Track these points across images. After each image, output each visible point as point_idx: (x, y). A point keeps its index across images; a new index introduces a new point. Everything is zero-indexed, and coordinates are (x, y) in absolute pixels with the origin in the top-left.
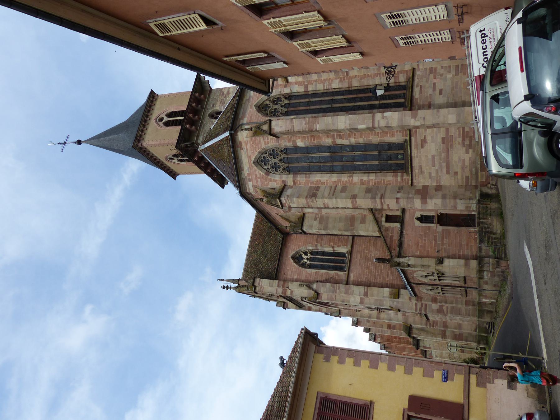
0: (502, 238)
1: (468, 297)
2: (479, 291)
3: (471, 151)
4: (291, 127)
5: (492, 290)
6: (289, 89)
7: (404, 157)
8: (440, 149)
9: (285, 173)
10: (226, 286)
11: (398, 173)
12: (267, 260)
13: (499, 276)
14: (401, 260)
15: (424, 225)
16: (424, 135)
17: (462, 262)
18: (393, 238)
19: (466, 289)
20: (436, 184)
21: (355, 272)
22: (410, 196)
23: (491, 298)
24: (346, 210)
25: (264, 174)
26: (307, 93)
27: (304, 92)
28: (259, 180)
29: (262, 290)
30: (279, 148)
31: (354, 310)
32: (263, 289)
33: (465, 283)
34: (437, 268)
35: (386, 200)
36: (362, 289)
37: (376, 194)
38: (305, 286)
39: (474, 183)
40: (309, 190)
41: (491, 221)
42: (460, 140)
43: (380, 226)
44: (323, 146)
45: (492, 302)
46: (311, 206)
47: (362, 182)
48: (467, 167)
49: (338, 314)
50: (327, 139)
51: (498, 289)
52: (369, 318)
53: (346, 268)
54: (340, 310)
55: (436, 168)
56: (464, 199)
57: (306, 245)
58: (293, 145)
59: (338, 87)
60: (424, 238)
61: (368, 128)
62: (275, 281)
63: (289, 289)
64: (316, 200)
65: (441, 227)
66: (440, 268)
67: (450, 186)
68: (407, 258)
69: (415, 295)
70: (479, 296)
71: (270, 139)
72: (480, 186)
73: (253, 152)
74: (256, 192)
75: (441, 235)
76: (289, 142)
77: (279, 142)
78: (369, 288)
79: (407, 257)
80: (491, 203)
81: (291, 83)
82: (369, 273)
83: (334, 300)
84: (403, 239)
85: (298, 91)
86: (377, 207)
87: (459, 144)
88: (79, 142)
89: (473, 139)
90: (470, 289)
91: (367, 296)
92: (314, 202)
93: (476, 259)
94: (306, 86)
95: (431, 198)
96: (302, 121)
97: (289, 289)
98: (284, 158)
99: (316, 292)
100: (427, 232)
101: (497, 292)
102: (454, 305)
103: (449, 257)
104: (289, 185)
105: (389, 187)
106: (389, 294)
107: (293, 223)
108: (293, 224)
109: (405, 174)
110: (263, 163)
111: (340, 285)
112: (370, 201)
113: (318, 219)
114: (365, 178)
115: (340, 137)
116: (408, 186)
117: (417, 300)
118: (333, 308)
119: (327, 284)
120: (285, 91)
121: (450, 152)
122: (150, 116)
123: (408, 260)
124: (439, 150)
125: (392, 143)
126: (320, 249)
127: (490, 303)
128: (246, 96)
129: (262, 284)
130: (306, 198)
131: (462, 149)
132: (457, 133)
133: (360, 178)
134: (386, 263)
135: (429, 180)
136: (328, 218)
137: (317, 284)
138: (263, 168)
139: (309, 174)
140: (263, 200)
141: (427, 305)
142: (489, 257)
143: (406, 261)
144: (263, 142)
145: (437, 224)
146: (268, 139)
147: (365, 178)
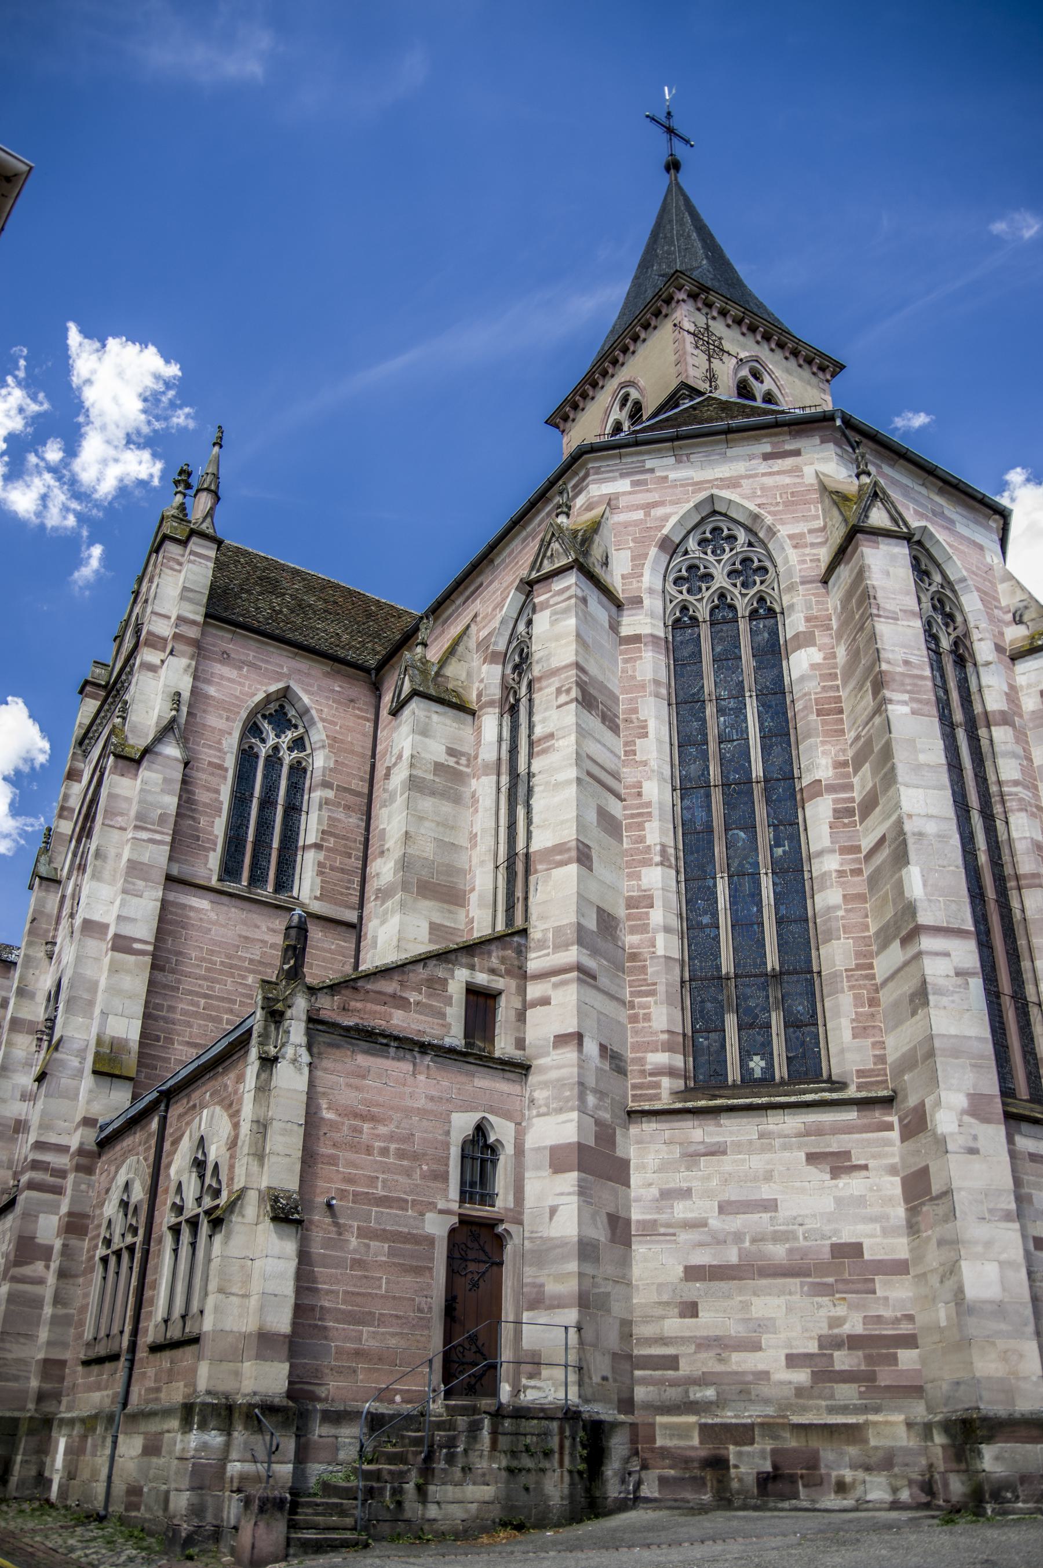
0: (401, 1527)
1: (80, 1368)
2: (110, 1419)
3: (802, 1376)
4: (888, 606)
5: (110, 1477)
6: (990, 659)
7: (755, 1080)
8: (805, 1238)
9: (668, 612)
10: (190, 480)
11: (681, 1057)
12: (281, 612)
13: (197, 1510)
14: (297, 1031)
15: (455, 1152)
16: (872, 1163)
17: (282, 1322)
18: (398, 1007)
19: (122, 1359)
20: (638, 1221)
21: (213, 916)
22: (591, 1100)
23: (71, 1474)
24: (492, 866)
25: (665, 531)
26: (981, 721)
27: (986, 713)
28: (642, 517)
29: (171, 563)
30: (773, 589)
31: (54, 937)
32: (175, 570)
33: (155, 1348)
34: (252, 1197)
35: (573, 988)
36: (144, 930)
37: (595, 952)
38: (174, 713)
39: (641, 1393)
40: (606, 687)
41: (484, 1475)
42: (854, 1325)
43: (453, 957)
44: (794, 753)
45: (50, 1481)
46: (540, 689)
47: (643, 901)
48: (721, 1360)
49: (44, 875)
50: (830, 761)
51: (117, 1508)
52: (18, 987)
53: (230, 887)
54: (58, 882)
55: (711, 1221)
56: (581, 1342)
57: (331, 746)
58: (797, 636)
59: (1015, 834)
60: (393, 1146)
61: (910, 909)
62: (203, 610)
63: (163, 662)
64: (567, 703)
65: (446, 1234)
66: (251, 1208)
67: (629, 1284)
68: (305, 1058)
69: (105, 1143)
70: (83, 1421)
71: (815, 555)
72: (631, 1424)
73: (759, 493)
74: (589, 507)
75: (406, 1230)
76: (808, 619)
77: (803, 583)
78: (148, 959)
79: (311, 1055)
80: (566, 1474)
81: (1013, 671)
82: (208, 970)
83: (107, 822)
84: (392, 1050)
85: (986, 692)
86: (532, 955)
87: (835, 1322)
88: (673, 166)
89: (863, 1389)
90: (121, 1375)
91: (114, 949)
92: (557, 697)
93: (290, 1394)
94: (1005, 719)
95: (583, 1191)
96: (916, 652)
97: (163, 662)
98: (732, 608)
99: (146, 751)
100: (425, 1167)
101: (99, 1504)
102: (48, 1311)
103: (304, 1257)
104: (623, 623)
105: (623, 1015)
106: (114, 1037)
107: (440, 668)
108: (435, 669)
109: (680, 1085)
110: (708, 535)
111: (168, 848)
112: (565, 922)
113: (451, 762)
114: (657, 916)
115: (842, 813)
116: (627, 1094)
117: (81, 1152)
118: (70, 855)
119: (176, 800)
120: (982, 643)
121: (794, 1283)
122: (766, 346)
123: (294, 1061)
124: (800, 1231)
125: (821, 1030)
126: (315, 796)
127: (47, 1474)
128: (951, 508)
129: (193, 562)
130: (578, 666)
131: (811, 1338)
132: (887, 1313)
133: (661, 892)
134: (284, 963)
135: (654, 1191)
136: (457, 799)
137: (177, 759)
138: (689, 533)
139: (669, 700)
140: (562, 513)
141: (56, 1197)
142: (301, 1458)
143: (289, 1051)
144: (801, 528)
145: (460, 1215)
146: (813, 545)
147: (657, 916)
